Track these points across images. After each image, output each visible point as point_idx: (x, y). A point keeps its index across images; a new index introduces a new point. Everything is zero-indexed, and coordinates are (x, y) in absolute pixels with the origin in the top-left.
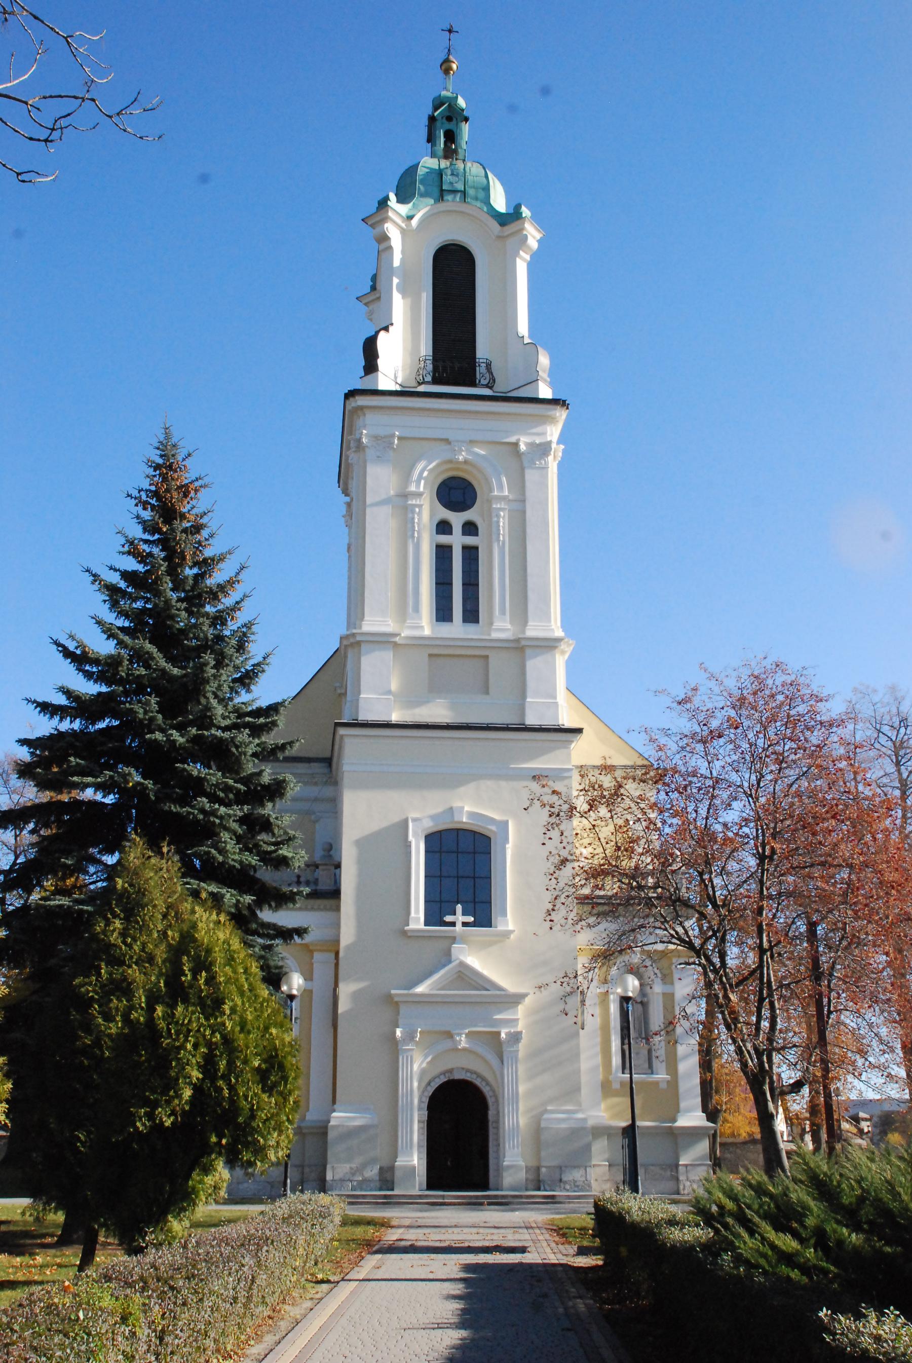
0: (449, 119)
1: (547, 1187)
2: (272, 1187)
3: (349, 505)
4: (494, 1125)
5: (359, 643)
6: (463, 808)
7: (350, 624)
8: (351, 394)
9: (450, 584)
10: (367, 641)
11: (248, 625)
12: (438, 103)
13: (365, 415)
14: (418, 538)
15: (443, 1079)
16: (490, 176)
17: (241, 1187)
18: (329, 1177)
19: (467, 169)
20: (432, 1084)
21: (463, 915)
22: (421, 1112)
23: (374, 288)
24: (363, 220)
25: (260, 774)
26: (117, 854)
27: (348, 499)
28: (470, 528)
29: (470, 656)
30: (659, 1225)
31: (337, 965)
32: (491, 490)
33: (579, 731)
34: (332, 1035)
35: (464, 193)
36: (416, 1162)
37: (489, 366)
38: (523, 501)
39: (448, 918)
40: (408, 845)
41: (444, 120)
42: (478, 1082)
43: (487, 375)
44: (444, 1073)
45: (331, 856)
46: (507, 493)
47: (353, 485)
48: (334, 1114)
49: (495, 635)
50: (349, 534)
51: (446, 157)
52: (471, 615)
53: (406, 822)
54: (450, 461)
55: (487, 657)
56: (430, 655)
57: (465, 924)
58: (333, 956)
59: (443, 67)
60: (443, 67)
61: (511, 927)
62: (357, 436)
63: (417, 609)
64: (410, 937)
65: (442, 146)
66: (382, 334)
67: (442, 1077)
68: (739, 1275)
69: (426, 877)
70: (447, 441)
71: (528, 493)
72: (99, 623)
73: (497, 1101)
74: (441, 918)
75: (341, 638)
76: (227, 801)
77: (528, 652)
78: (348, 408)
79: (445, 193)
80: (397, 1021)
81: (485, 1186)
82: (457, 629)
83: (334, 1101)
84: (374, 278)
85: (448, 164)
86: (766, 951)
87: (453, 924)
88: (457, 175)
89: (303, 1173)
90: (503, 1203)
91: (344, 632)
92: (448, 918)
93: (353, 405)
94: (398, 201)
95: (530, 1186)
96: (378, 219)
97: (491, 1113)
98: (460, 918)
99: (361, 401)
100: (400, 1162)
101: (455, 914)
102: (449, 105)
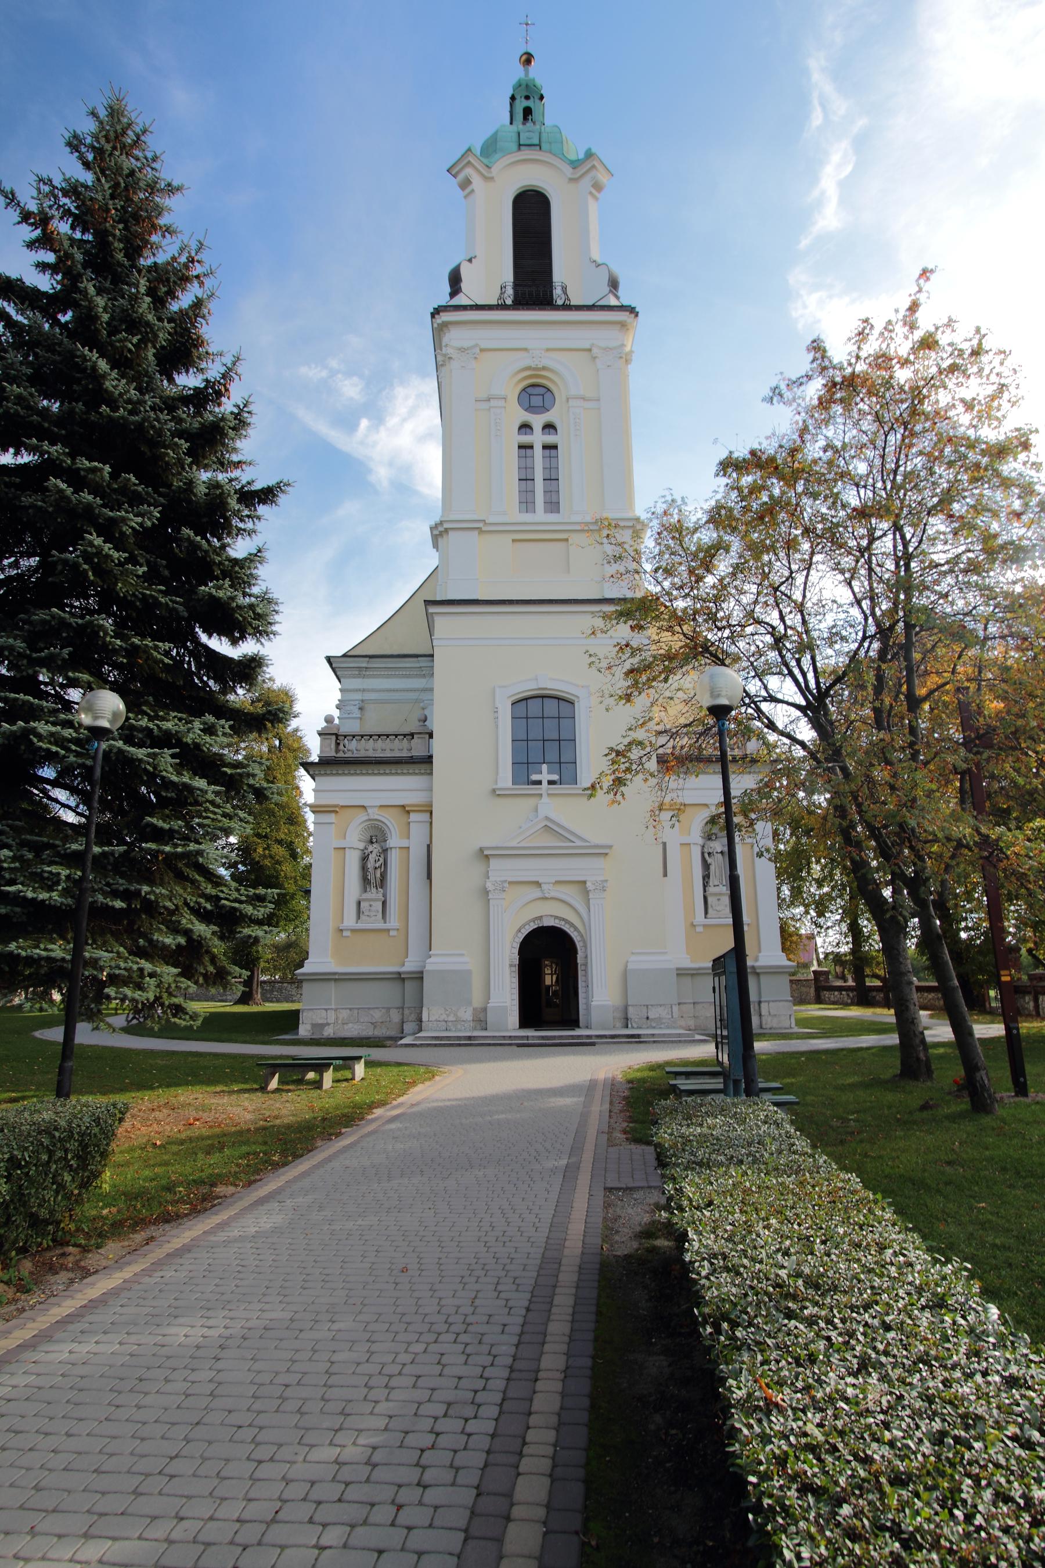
0: (527, 98)
1: (635, 1025)
2: (375, 1027)
4: (583, 968)
8: (436, 312)
12: (519, 85)
15: (533, 926)
17: (346, 1027)
18: (425, 1017)
20: (523, 931)
21: (549, 773)
22: (513, 969)
28: (549, 427)
30: (208, 952)
37: (564, 290)
39: (535, 777)
42: (566, 928)
43: (563, 296)
44: (533, 920)
48: (428, 961)
52: (553, 505)
55: (567, 540)
56: (514, 541)
57: (550, 782)
67: (532, 924)
68: (869, 864)
73: (585, 946)
75: (431, 528)
81: (574, 1023)
87: (539, 783)
89: (403, 1014)
90: (587, 1043)
95: (619, 1024)
97: (580, 959)
99: (445, 317)
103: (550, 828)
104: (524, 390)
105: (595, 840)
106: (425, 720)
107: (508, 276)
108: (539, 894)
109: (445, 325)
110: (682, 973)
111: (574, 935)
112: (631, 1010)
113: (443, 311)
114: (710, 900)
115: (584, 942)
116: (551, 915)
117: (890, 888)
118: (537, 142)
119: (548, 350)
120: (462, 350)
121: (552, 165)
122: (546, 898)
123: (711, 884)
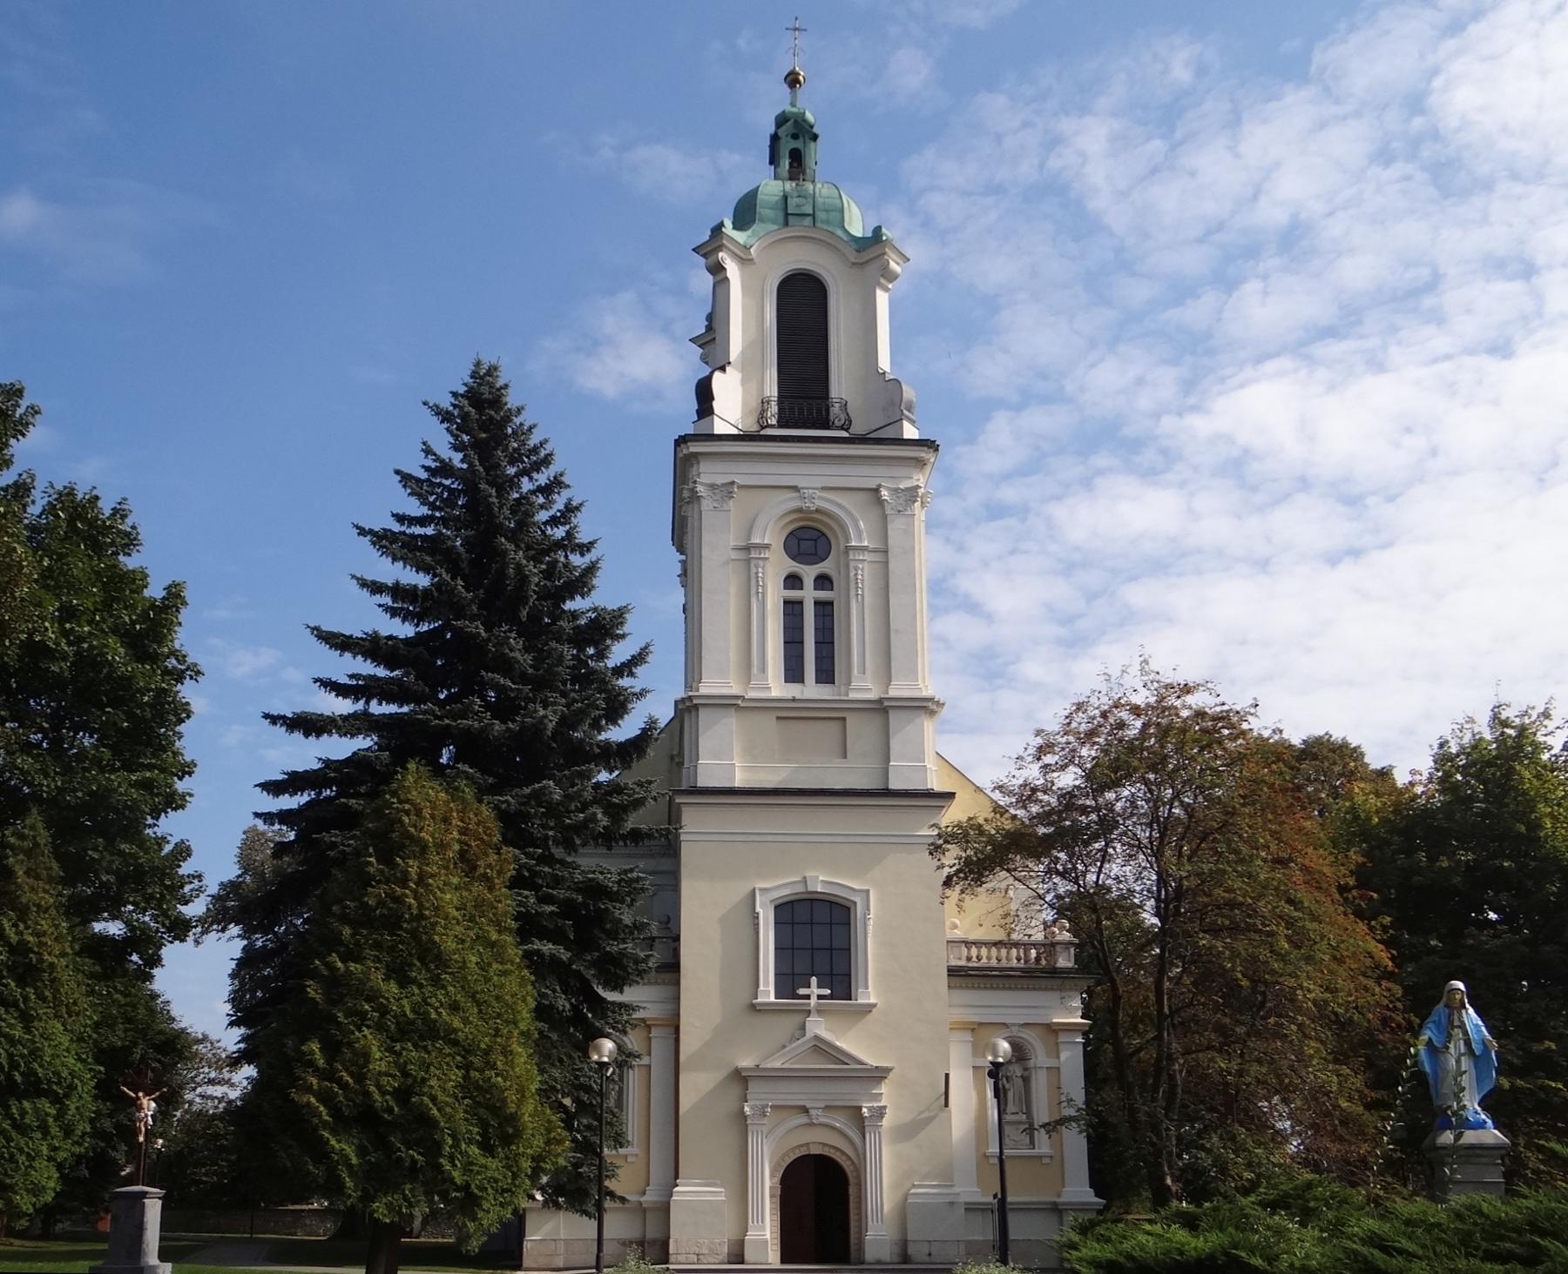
0: (795, 137)
3: (684, 563)
5: (696, 707)
6: (818, 877)
7: (688, 686)
8: (681, 441)
9: (801, 629)
10: (730, 250)
11: (551, 455)
12: (782, 120)
13: (699, 463)
14: (763, 593)
16: (844, 198)
19: (817, 191)
21: (819, 987)
22: (774, 1200)
23: (709, 328)
24: (694, 250)
25: (593, 975)
26: (362, 702)
27: (683, 557)
28: (823, 581)
29: (824, 719)
31: (677, 1040)
32: (848, 539)
33: (951, 795)
34: (672, 1041)
35: (813, 216)
36: (768, 1236)
38: (886, 552)
39: (802, 991)
40: (755, 917)
41: (789, 138)
45: (669, 928)
46: (866, 544)
47: (688, 540)
48: (676, 1189)
49: (853, 695)
50: (686, 595)
51: (791, 179)
52: (826, 675)
53: (754, 889)
54: (800, 510)
55: (844, 719)
56: (778, 718)
57: (820, 997)
58: (672, 1030)
59: (788, 79)
60: (788, 79)
61: (872, 1000)
62: (691, 485)
63: (763, 669)
64: (759, 1010)
65: (787, 167)
66: (717, 375)
69: (776, 974)
70: (795, 488)
71: (891, 542)
72: (376, 588)
74: (794, 990)
75: (676, 702)
76: (555, 917)
77: (893, 715)
78: (680, 455)
79: (790, 217)
80: (746, 1096)
82: (810, 689)
83: (677, 1177)
84: (710, 318)
85: (794, 185)
86: (1167, 1017)
87: (808, 997)
88: (805, 197)
91: (681, 694)
92: (802, 991)
93: (685, 451)
94: (734, 228)
96: (713, 246)
98: (814, 990)
99: (694, 448)
100: (751, 1235)
101: (809, 987)
102: (796, 122)
103: (822, 1048)
104: (791, 533)
105: (873, 1062)
106: (668, 922)
107: (772, 390)
108: (808, 1121)
109: (695, 456)
110: (971, 1208)
111: (845, 1164)
112: (910, 1245)
113: (691, 441)
114: (1007, 1129)
115: (857, 1170)
116: (817, 1141)
117: (1153, 780)
118: (811, 212)
119: (824, 489)
120: (712, 486)
121: (837, 248)
122: (814, 1124)
123: (1008, 1111)
